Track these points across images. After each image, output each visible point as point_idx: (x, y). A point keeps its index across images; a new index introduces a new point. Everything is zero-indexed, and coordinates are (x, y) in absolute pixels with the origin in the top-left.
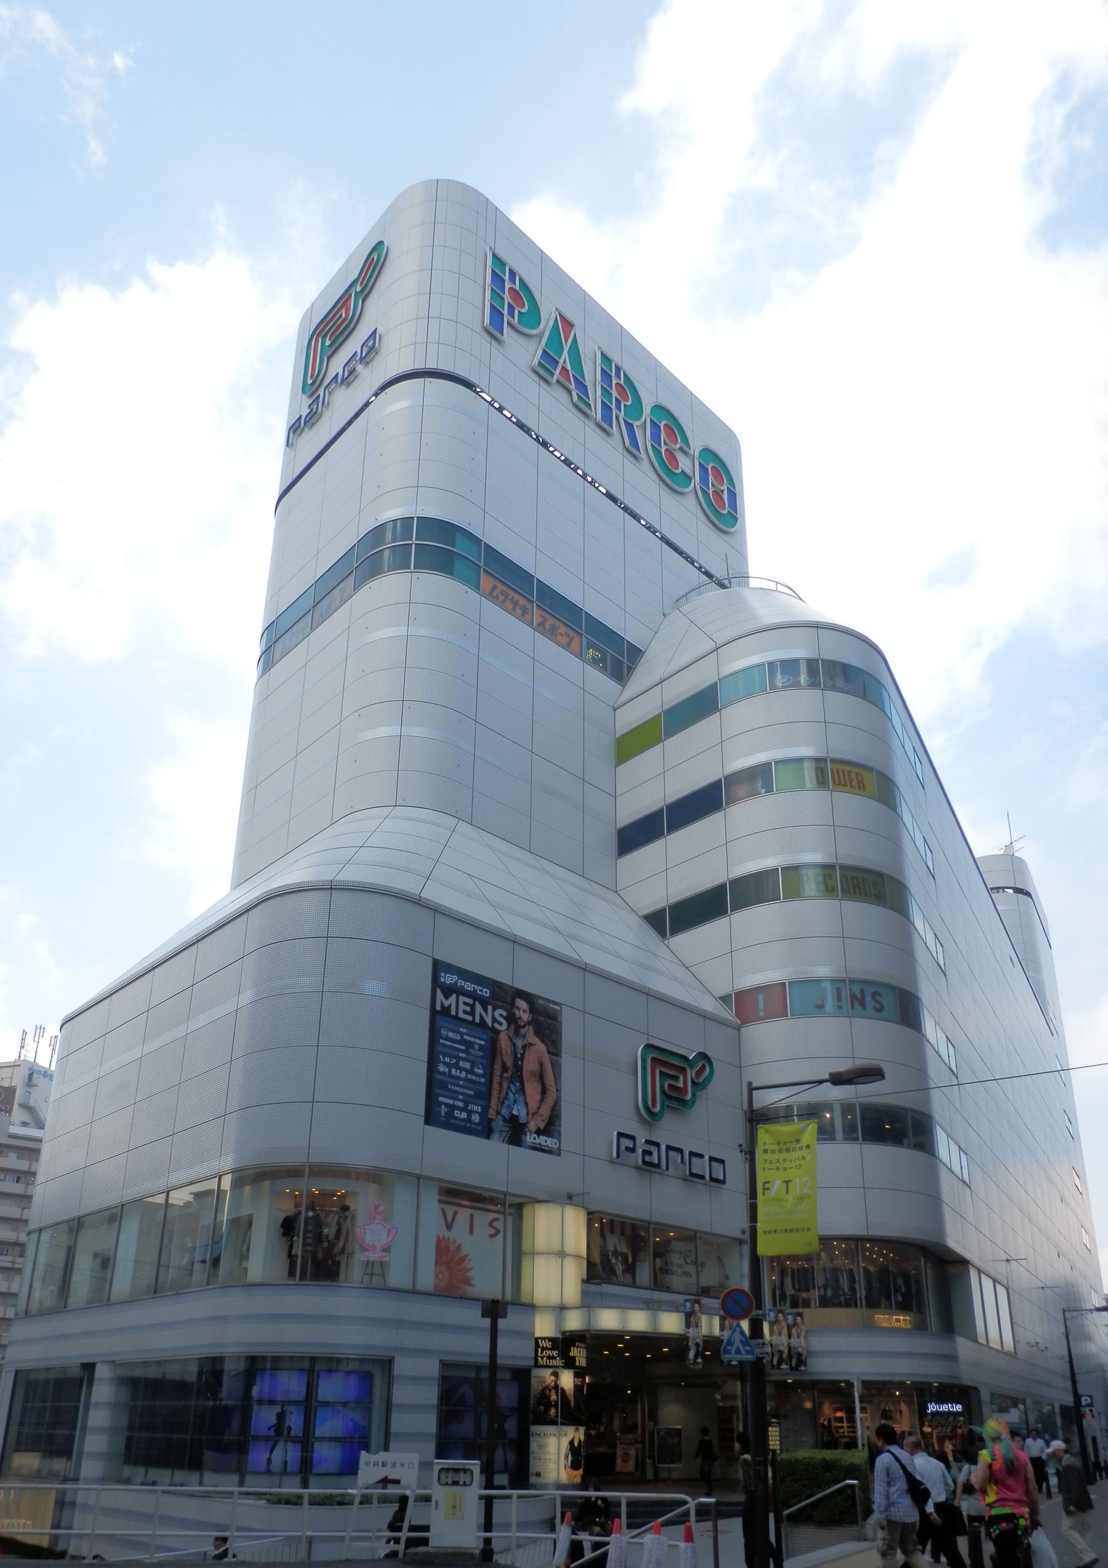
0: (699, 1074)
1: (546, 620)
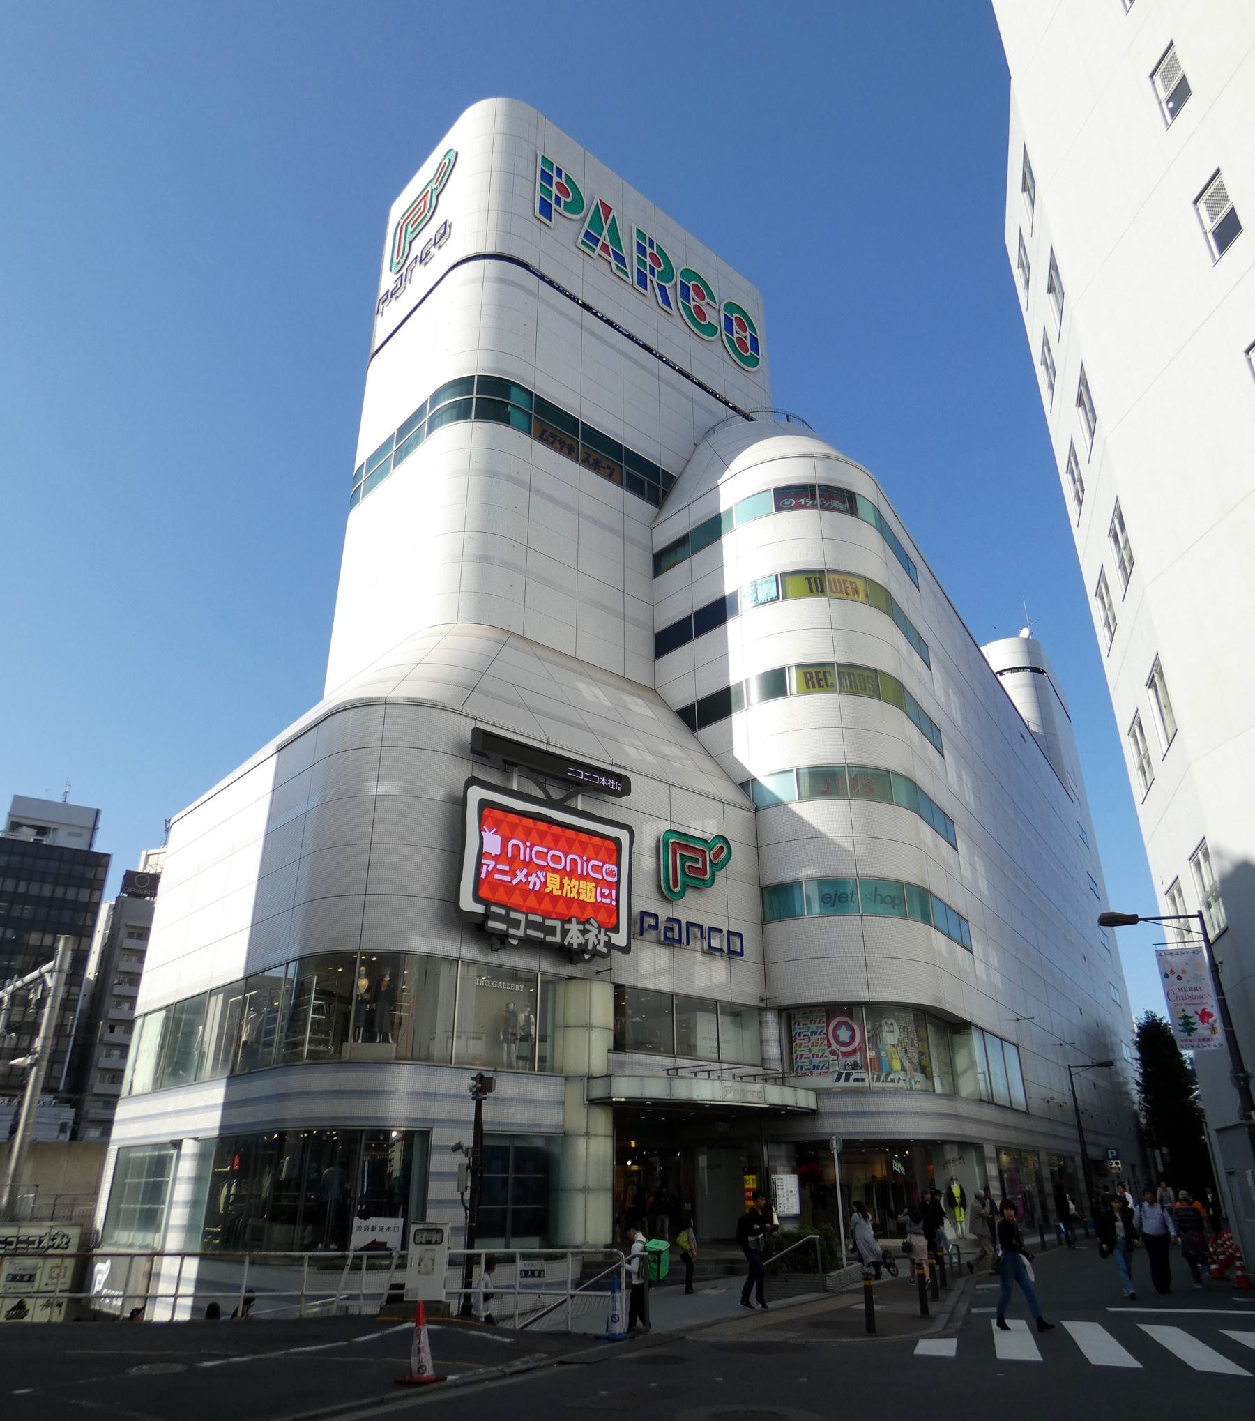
0: (717, 855)
1: (589, 456)
